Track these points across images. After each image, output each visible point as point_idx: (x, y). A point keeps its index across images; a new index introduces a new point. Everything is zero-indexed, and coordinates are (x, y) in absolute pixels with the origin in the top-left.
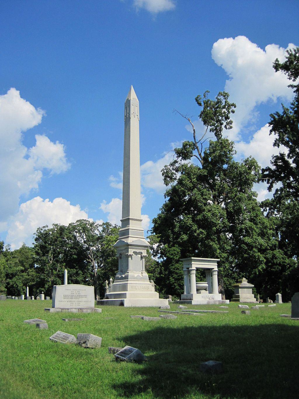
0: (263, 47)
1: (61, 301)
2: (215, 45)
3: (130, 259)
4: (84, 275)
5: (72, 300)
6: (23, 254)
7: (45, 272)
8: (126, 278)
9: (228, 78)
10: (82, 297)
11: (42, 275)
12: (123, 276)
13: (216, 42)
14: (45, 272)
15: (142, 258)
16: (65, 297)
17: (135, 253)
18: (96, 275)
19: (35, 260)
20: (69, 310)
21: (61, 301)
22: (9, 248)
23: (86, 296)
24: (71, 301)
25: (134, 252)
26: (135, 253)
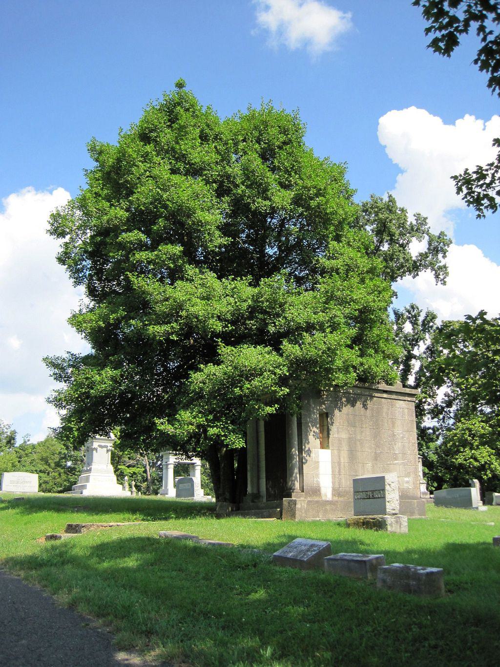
0: (454, 124)
1: (8, 486)
2: (382, 120)
3: (94, 452)
4: (133, 477)
5: (18, 485)
6: (48, 447)
7: (76, 473)
8: (90, 470)
9: (401, 171)
10: (27, 482)
11: (73, 477)
12: (88, 468)
13: (398, 110)
14: (76, 473)
15: (108, 451)
16: (12, 482)
17: (100, 446)
18: (149, 478)
19: (63, 456)
20: (15, 493)
21: (8, 486)
22: (28, 438)
23: (30, 482)
24: (16, 486)
25: (99, 446)
26: (100, 446)
